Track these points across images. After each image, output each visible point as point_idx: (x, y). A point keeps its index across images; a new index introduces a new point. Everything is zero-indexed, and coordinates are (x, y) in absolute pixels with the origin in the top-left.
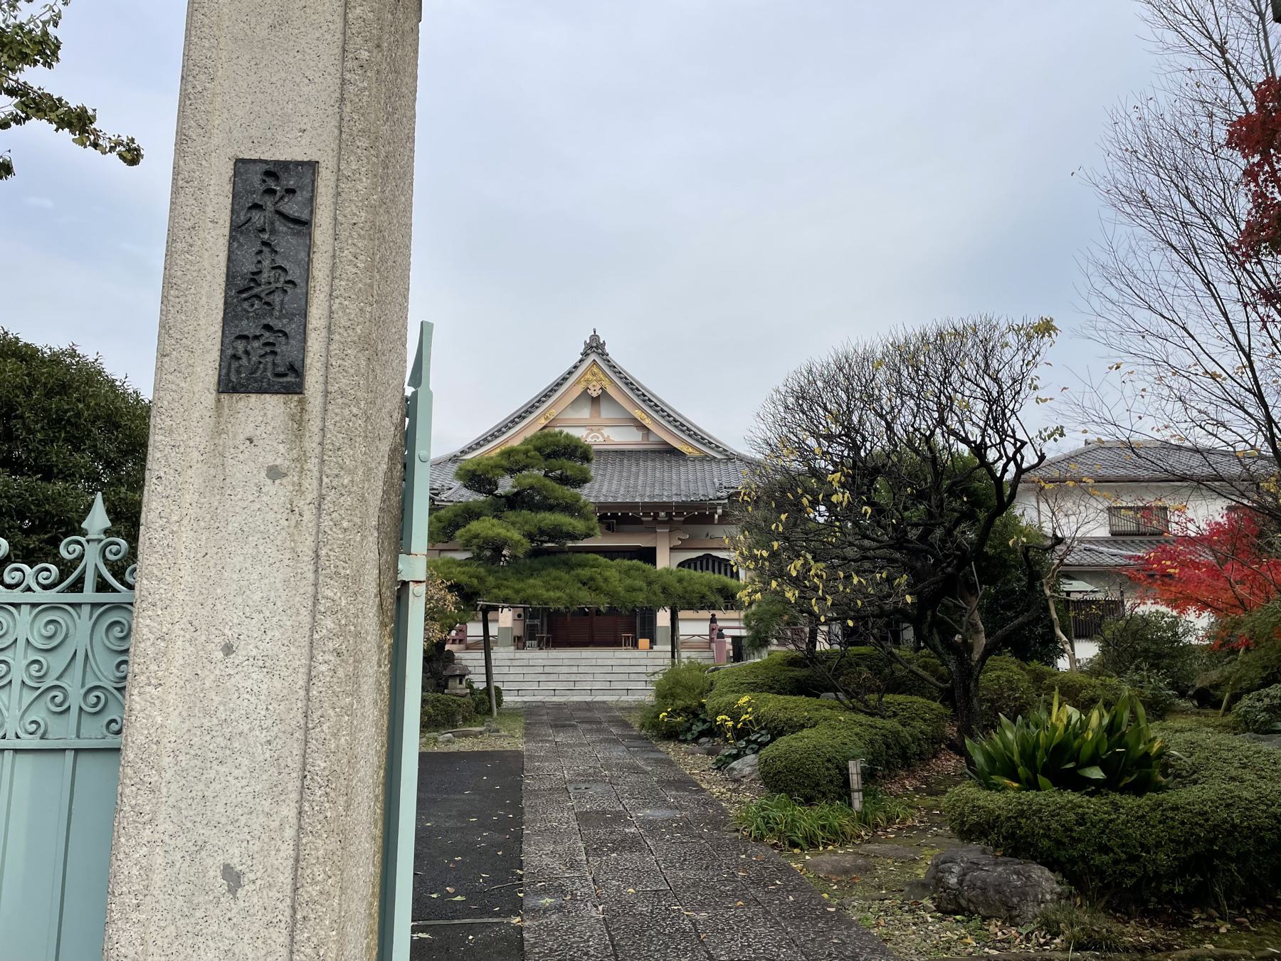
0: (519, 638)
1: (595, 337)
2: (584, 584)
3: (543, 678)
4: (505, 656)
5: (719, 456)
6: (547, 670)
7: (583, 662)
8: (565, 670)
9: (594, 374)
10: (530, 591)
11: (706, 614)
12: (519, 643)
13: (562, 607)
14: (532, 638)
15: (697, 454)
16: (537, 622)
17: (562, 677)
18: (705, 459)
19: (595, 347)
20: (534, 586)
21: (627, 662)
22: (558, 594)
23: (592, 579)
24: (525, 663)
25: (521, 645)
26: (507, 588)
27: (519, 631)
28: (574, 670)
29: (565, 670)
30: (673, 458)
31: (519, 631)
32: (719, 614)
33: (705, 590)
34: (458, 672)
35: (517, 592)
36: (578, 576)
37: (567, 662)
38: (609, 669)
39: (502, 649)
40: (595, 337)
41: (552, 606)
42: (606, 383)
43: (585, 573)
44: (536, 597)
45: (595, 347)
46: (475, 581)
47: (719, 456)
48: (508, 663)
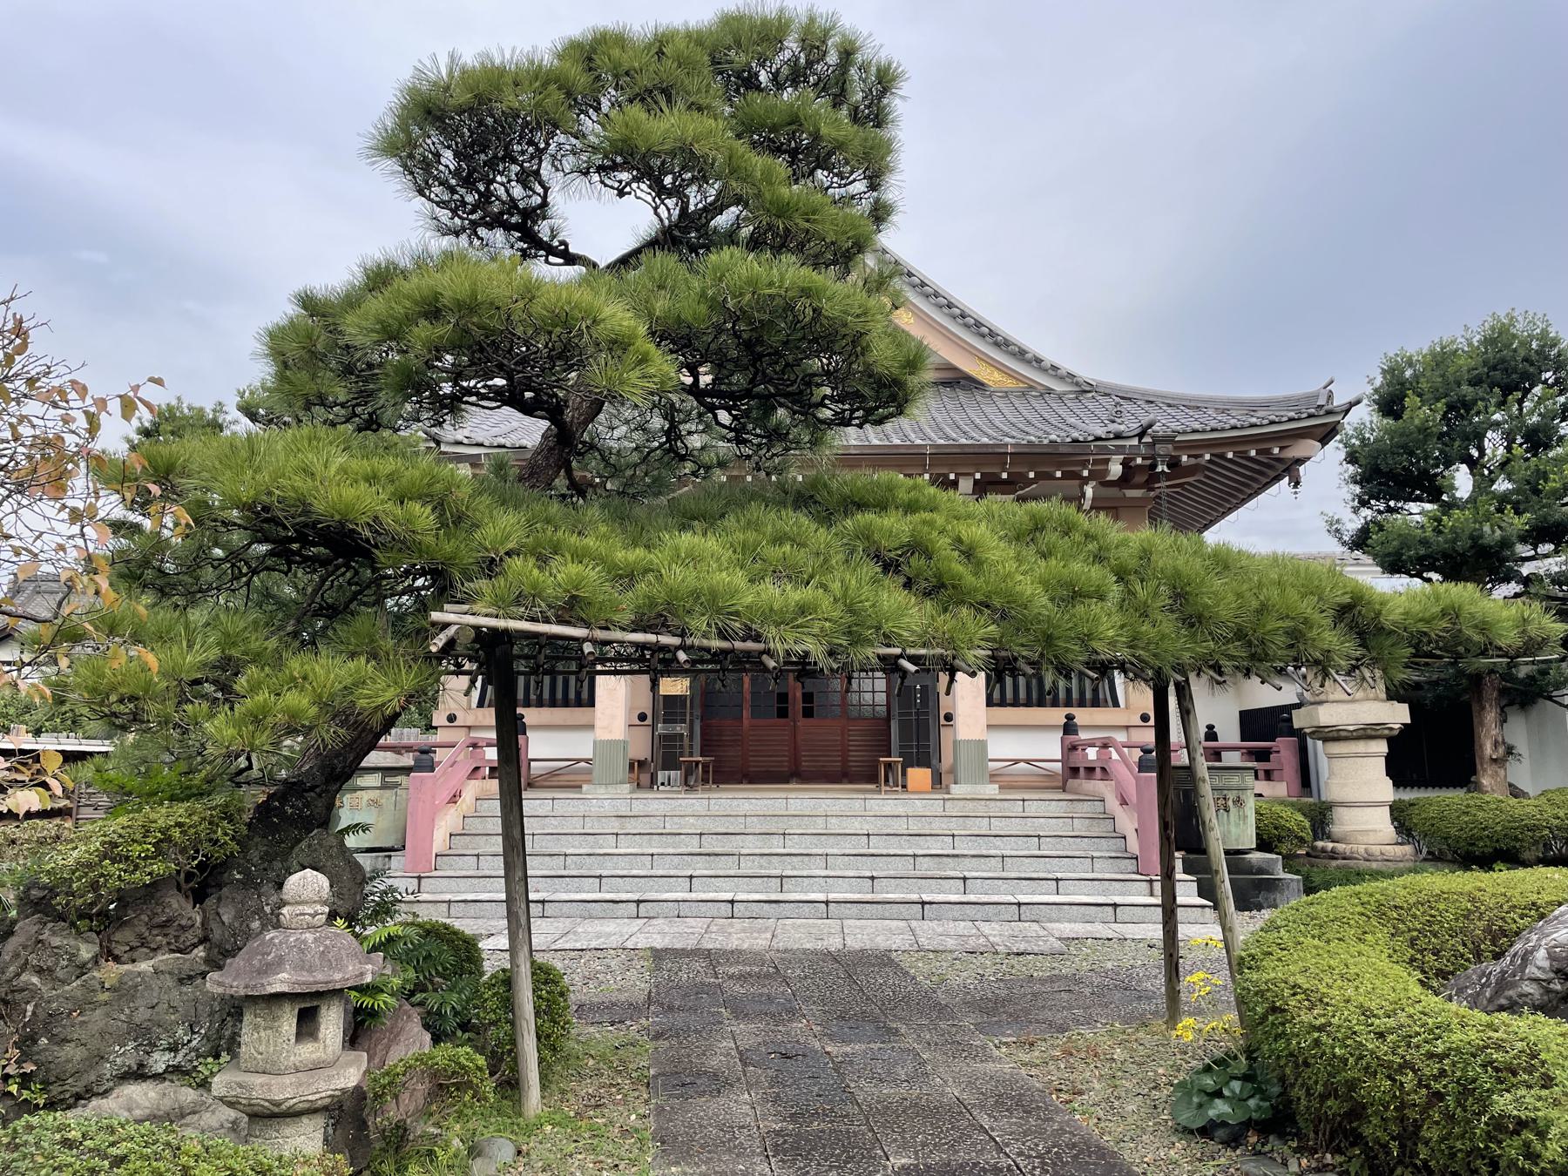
0: (642, 764)
2: (890, 566)
3: (700, 867)
4: (607, 807)
5: (1058, 387)
6: (711, 844)
7: (794, 827)
8: (751, 845)
10: (680, 577)
11: (1057, 715)
12: (642, 773)
13: (815, 649)
14: (669, 763)
15: (1010, 384)
16: (681, 729)
17: (748, 867)
18: (1028, 390)
20: (694, 558)
21: (899, 826)
22: (796, 595)
23: (918, 547)
24: (655, 825)
25: (645, 778)
26: (579, 556)
27: (641, 750)
28: (776, 846)
29: (751, 845)
30: (962, 396)
31: (641, 748)
32: (1083, 716)
33: (1307, 607)
34: (280, 982)
35: (627, 577)
36: (865, 535)
37: (756, 825)
38: (860, 846)
39: (601, 791)
41: (781, 643)
43: (893, 526)
44: (711, 601)
46: (423, 516)
47: (1058, 387)
48: (615, 826)
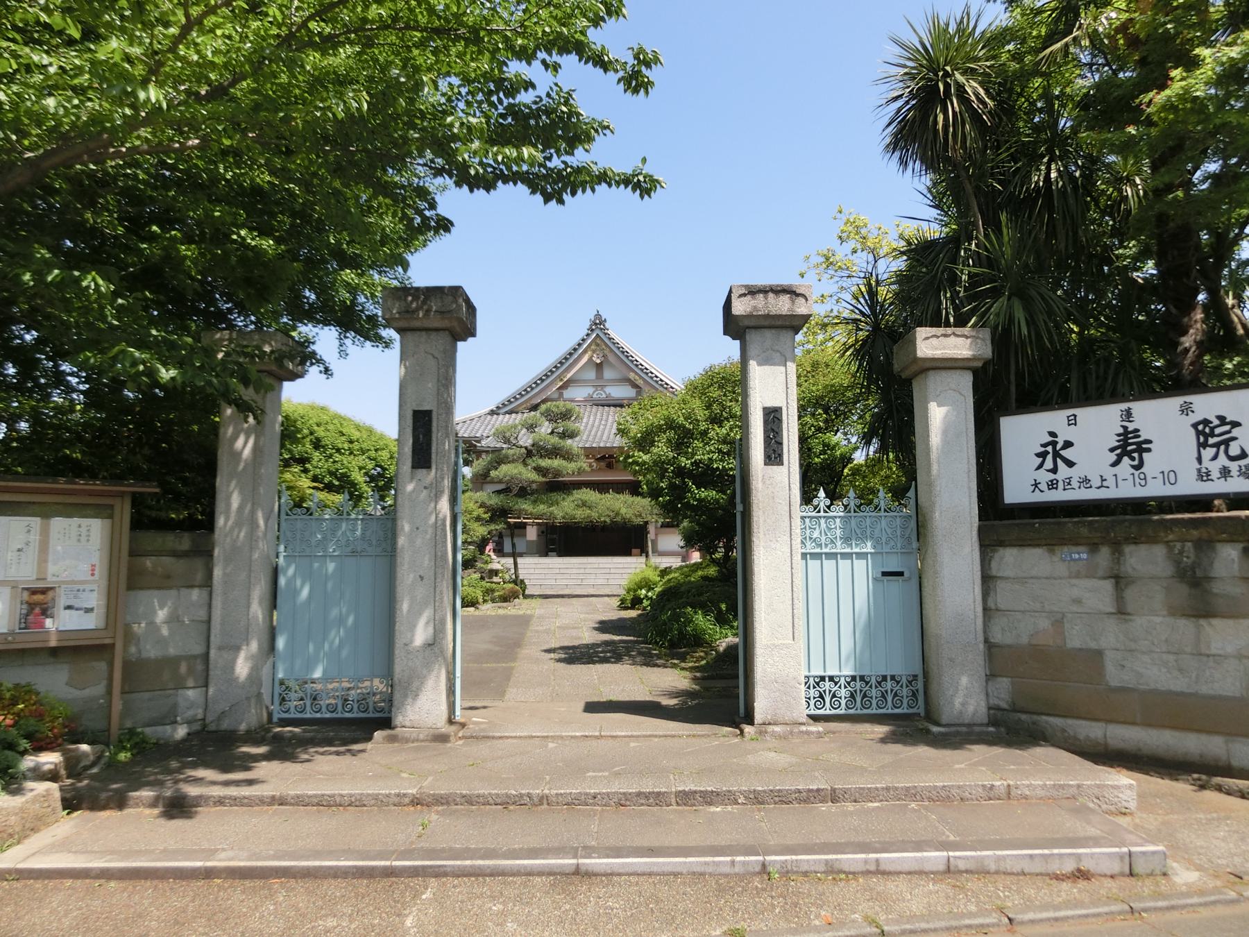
1: (598, 315)
3: (559, 577)
9: (598, 345)
19: (598, 323)
40: (598, 315)
42: (607, 352)
45: (598, 323)
